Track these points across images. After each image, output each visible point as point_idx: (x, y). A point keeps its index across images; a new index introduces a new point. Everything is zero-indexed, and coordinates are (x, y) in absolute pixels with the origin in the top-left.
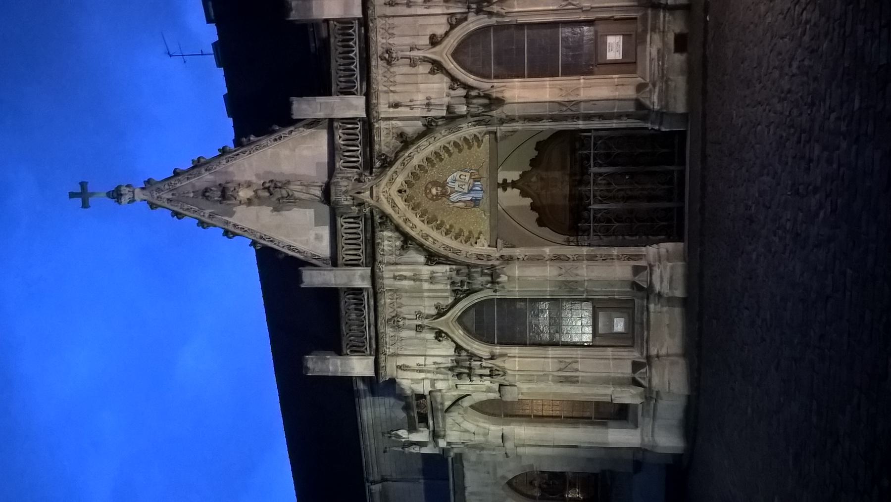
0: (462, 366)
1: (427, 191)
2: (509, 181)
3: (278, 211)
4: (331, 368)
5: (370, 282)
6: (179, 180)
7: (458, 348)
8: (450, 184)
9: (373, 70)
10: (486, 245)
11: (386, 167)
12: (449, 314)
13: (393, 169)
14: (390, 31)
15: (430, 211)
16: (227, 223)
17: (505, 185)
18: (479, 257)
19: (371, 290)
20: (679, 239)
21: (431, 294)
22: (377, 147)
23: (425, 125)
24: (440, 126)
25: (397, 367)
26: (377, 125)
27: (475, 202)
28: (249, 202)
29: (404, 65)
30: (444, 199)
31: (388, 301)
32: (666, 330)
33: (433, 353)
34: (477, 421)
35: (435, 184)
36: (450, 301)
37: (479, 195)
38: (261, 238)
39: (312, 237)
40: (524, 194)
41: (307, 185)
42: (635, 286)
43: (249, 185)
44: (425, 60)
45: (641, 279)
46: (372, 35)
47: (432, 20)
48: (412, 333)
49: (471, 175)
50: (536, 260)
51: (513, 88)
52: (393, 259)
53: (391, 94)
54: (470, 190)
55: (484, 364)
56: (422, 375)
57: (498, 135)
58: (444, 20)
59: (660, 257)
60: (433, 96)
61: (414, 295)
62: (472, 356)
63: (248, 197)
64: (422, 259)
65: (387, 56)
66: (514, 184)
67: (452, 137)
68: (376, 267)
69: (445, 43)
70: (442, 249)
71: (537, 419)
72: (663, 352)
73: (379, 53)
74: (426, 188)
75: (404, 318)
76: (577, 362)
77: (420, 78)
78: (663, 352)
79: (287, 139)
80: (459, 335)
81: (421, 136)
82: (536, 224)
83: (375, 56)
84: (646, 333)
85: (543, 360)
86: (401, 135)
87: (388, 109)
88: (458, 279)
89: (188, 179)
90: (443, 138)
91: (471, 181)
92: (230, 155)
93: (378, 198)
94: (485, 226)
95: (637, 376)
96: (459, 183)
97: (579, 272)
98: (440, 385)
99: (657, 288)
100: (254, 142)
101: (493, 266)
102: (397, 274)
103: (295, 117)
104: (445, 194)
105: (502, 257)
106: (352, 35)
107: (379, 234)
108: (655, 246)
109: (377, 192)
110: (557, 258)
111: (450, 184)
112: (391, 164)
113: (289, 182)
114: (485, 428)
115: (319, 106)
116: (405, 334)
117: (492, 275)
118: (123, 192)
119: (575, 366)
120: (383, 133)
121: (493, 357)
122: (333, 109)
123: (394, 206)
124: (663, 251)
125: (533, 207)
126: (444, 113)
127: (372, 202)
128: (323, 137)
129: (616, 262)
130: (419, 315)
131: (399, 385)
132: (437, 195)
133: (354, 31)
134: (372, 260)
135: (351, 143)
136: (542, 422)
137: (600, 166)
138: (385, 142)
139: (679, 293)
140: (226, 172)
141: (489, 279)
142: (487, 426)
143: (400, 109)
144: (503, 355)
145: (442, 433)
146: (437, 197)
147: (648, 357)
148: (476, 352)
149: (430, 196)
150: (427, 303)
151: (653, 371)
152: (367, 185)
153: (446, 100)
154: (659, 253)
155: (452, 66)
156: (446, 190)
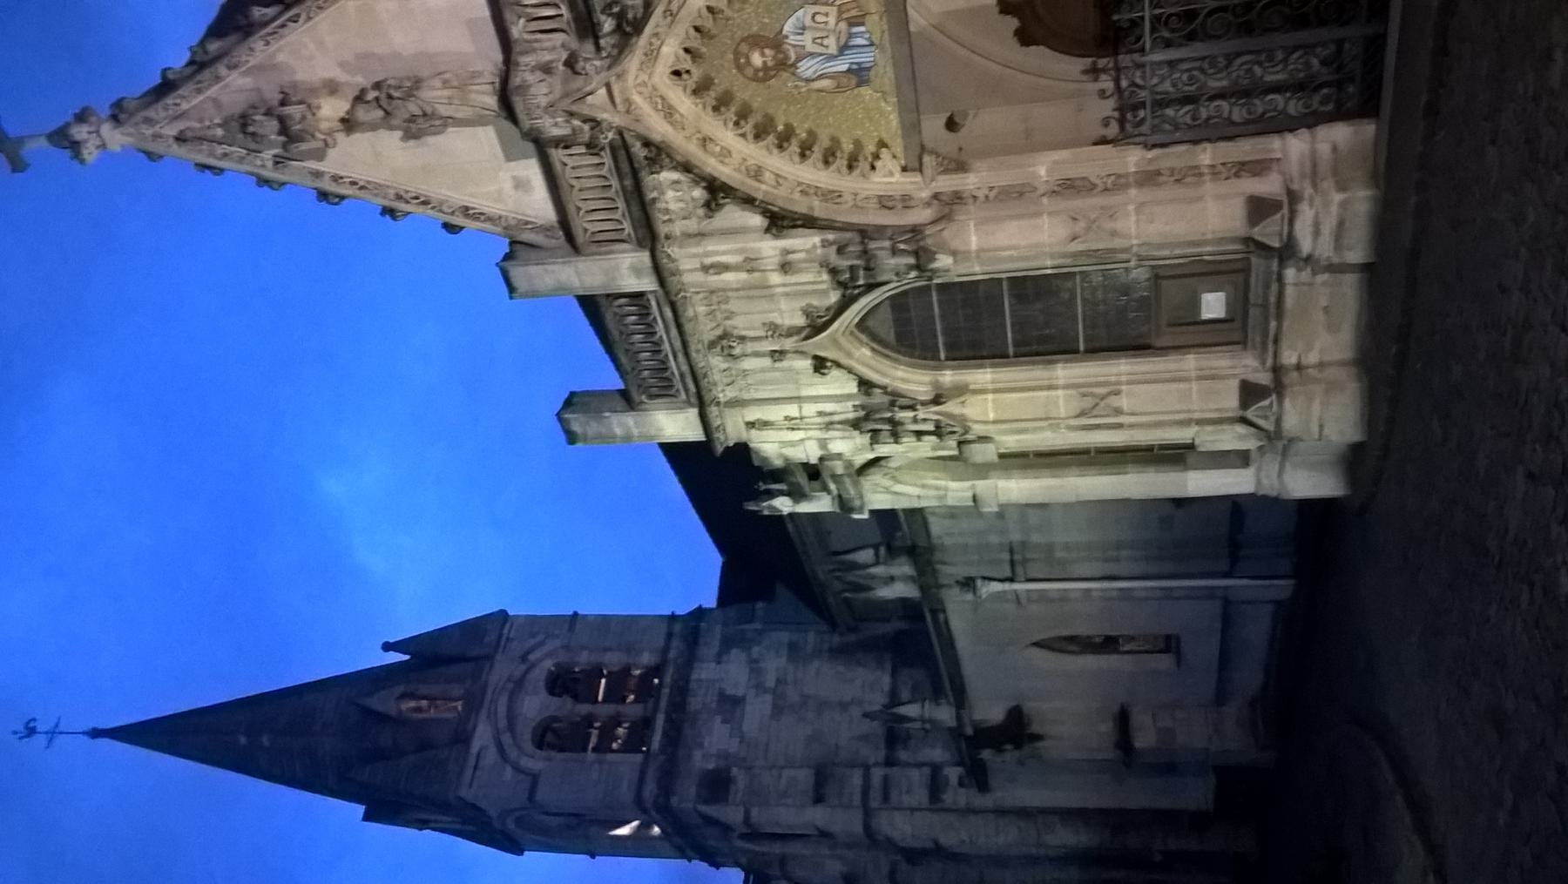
0: (878, 415)
6: (183, 97)
7: (865, 385)
8: (793, 39)
12: (836, 325)
15: (755, 105)
16: (318, 175)
18: (885, 203)
19: (661, 292)
20: (1366, 108)
21: (787, 289)
27: (860, 75)
28: (348, 124)
30: (785, 75)
31: (702, 309)
32: (1320, 316)
34: (921, 478)
35: (756, 41)
36: (834, 297)
37: (866, 58)
38: (399, 197)
39: (508, 186)
41: (462, 85)
42: (1253, 244)
43: (332, 88)
45: (1269, 230)
49: (840, 12)
50: (1016, 196)
52: (692, 225)
54: (844, 49)
55: (921, 415)
59: (1314, 165)
61: (752, 293)
62: (896, 399)
63: (342, 114)
68: (658, 254)
70: (797, 196)
72: (1312, 358)
74: (737, 54)
75: (742, 339)
76: (1118, 393)
78: (1312, 358)
80: (864, 357)
82: (1014, 43)
84: (1273, 324)
85: (1045, 393)
88: (844, 263)
91: (843, 26)
92: (269, 29)
94: (890, 121)
95: (1250, 414)
97: (1118, 225)
98: (838, 446)
99: (1305, 245)
101: (916, 231)
102: (708, 261)
104: (784, 65)
105: (936, 196)
107: (649, 180)
108: (1304, 133)
109: (623, 91)
110: (1069, 187)
112: (638, 26)
113: (418, 83)
114: (937, 488)
116: (748, 364)
117: (916, 254)
118: (78, 137)
119: (1114, 401)
123: (669, 112)
124: (1324, 149)
127: (617, 120)
129: (1209, 187)
130: (774, 330)
132: (765, 67)
134: (648, 235)
136: (1049, 466)
137: (1168, 44)
139: (1357, 254)
140: (275, 67)
141: (911, 260)
142: (942, 483)
144: (961, 390)
147: (1277, 370)
149: (749, 72)
151: (1287, 403)
152: (597, 80)
154: (1313, 152)
156: (787, 57)
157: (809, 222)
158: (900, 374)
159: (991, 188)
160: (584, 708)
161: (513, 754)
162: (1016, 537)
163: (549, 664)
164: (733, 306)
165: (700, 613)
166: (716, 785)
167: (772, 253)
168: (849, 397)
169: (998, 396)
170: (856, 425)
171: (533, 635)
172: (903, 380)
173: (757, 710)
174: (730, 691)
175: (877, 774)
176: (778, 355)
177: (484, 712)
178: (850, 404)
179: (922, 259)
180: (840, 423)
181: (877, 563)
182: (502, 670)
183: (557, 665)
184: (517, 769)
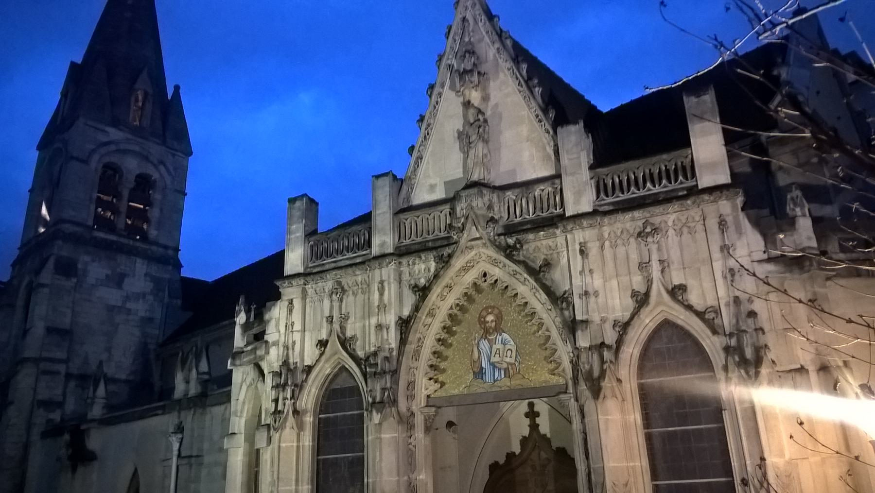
0: (290, 376)
1: (488, 309)
2: (538, 420)
3: (459, 138)
4: (294, 227)
5: (378, 254)
6: (485, 23)
7: (309, 369)
8: (499, 338)
9: (628, 216)
10: (428, 392)
11: (505, 251)
13: (507, 262)
14: (685, 230)
15: (467, 315)
17: (532, 414)
18: (411, 385)
22: (531, 236)
23: (565, 292)
24: (562, 315)
25: (292, 300)
26: (558, 232)
27: (479, 374)
28: (467, 104)
29: (641, 255)
31: (359, 278)
33: (307, 339)
35: (499, 318)
36: (361, 354)
37: (488, 377)
38: (429, 125)
39: (433, 181)
40: (524, 441)
41: (485, 165)
43: (486, 98)
44: (649, 282)
46: (676, 206)
47: (707, 285)
48: (327, 313)
49: (511, 364)
51: (623, 412)
52: (406, 277)
53: (597, 243)
54: (493, 365)
55: (288, 402)
56: (282, 330)
57: (562, 396)
58: (711, 301)
60: (601, 299)
62: (299, 387)
63: (472, 102)
64: (406, 313)
65: (648, 230)
66: (534, 427)
67: (555, 334)
68: (391, 257)
69: (677, 307)
70: (418, 335)
71: (253, 476)
73: (651, 220)
74: (493, 307)
75: (341, 301)
77: (625, 279)
79: (539, 129)
80: (325, 369)
81: (549, 291)
83: (648, 215)
85: (294, 478)
86: (547, 264)
87: (577, 242)
89: (487, 32)
90: (549, 317)
91: (505, 366)
93: (472, 248)
94: (454, 389)
96: (501, 349)
98: (273, 351)
100: (532, 92)
101: (394, 402)
102: (386, 284)
103: (559, 129)
104: (487, 332)
105: (413, 414)
106: (676, 181)
107: (431, 256)
111: (499, 338)
112: (509, 257)
113: (486, 142)
114: (241, 412)
115: (575, 156)
116: (326, 303)
117: (382, 402)
120: (550, 242)
121: (296, 412)
122: (573, 174)
123: (465, 269)
125: (510, 456)
126: (579, 317)
127: (463, 241)
128: (546, 171)
130: (345, 318)
131: (274, 305)
132: (486, 322)
133: (681, 183)
134: (402, 252)
135: (538, 205)
138: (538, 245)
140: (497, 72)
141: (378, 399)
143: (579, 257)
144: (300, 427)
145: (238, 362)
146: (482, 322)
148: (305, 392)
149: (484, 313)
150: (358, 325)
153: (596, 318)
155: (648, 321)
156: (490, 334)
157: (403, 341)
158: (313, 390)
159: (415, 446)
160: (126, 194)
161: (103, 150)
162: (207, 459)
163: (156, 176)
164: (360, 297)
165: (178, 266)
166: (67, 268)
167: (388, 319)
168: (302, 360)
169: (295, 449)
170: (286, 363)
171: (175, 169)
172: (310, 392)
173: (113, 296)
174: (126, 280)
175: (62, 368)
176: (330, 320)
177: (130, 136)
178: (298, 360)
179: (378, 405)
180: (287, 354)
181: (198, 373)
182: (155, 150)
183: (155, 181)
184: (93, 151)
